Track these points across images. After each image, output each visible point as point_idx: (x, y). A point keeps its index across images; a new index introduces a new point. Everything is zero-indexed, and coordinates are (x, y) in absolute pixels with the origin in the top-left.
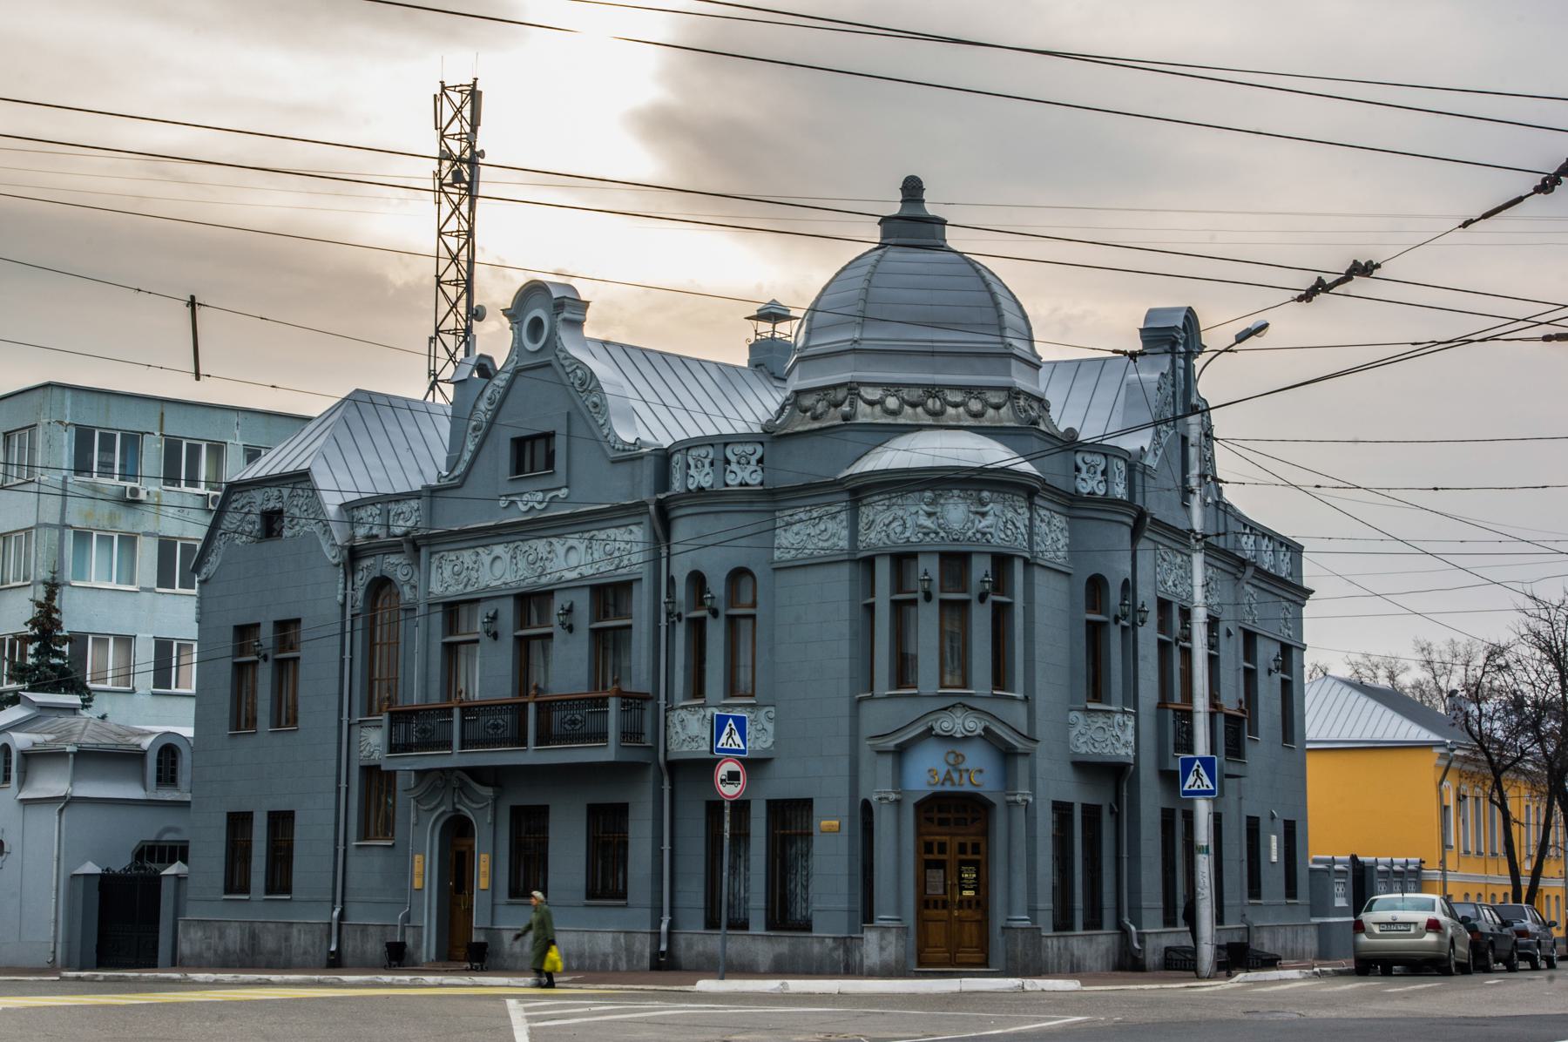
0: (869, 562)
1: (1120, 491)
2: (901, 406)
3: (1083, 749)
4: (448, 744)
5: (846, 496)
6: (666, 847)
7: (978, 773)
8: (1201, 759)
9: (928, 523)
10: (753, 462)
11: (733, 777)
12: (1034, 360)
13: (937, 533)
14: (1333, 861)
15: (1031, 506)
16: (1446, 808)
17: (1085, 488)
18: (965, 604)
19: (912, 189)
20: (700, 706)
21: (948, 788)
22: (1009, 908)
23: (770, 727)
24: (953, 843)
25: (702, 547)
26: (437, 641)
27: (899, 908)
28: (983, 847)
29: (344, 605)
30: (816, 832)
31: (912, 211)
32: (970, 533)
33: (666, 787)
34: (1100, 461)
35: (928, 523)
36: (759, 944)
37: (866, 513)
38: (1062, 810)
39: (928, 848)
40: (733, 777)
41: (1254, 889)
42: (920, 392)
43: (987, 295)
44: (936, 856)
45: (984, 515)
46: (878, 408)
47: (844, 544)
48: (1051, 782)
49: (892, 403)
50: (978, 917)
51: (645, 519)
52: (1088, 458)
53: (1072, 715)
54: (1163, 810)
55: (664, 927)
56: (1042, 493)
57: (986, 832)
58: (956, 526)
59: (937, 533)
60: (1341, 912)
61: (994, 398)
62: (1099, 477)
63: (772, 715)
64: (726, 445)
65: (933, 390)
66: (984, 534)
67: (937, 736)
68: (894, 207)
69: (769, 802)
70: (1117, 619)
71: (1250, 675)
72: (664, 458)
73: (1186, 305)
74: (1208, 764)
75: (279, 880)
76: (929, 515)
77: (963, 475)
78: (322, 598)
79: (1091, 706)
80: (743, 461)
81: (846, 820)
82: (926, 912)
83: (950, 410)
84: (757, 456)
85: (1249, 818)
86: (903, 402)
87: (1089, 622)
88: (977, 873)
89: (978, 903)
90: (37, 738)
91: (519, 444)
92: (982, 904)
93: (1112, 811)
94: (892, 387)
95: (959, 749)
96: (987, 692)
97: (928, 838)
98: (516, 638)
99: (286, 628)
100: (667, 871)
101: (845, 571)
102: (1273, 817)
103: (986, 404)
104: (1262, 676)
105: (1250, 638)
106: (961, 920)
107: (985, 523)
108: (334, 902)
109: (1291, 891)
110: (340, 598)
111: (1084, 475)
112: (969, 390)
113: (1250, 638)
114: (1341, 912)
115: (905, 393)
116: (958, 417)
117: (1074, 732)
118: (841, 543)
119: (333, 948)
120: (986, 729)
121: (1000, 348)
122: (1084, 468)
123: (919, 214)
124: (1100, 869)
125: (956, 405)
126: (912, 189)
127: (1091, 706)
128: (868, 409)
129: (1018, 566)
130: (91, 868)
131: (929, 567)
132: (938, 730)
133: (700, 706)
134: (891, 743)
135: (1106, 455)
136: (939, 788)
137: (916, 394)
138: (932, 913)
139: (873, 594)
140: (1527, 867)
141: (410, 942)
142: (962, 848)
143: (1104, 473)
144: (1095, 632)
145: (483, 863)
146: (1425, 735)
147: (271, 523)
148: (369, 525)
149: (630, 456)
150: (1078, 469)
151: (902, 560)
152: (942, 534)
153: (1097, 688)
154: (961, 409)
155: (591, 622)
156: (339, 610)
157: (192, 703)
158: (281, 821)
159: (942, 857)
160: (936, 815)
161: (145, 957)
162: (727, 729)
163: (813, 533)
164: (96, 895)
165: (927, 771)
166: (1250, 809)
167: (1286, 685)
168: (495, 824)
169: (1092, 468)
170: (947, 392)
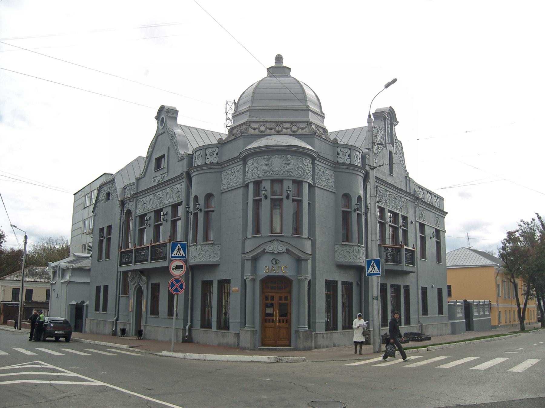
0: (247, 185)
1: (358, 162)
2: (266, 130)
3: (341, 260)
4: (131, 263)
6: (190, 298)
7: (285, 268)
8: (374, 260)
9: (266, 168)
10: (347, 156)
11: (179, 267)
12: (322, 115)
13: (270, 172)
14: (457, 302)
15: (313, 163)
16: (498, 285)
17: (341, 161)
19: (279, 59)
20: (195, 245)
22: (298, 322)
23: (219, 252)
24: (277, 296)
27: (253, 322)
28: (289, 298)
30: (231, 292)
31: (279, 65)
32: (282, 172)
33: (190, 276)
34: (347, 150)
35: (266, 168)
39: (267, 298)
40: (179, 267)
41: (425, 311)
42: (274, 124)
43: (301, 90)
44: (269, 301)
45: (288, 164)
46: (257, 131)
47: (241, 180)
48: (324, 271)
49: (262, 128)
50: (287, 326)
51: (184, 180)
52: (343, 150)
53: (336, 247)
54: (382, 285)
55: (187, 327)
56: (318, 159)
57: (290, 292)
58: (277, 169)
59: (270, 172)
60: (460, 318)
61: (302, 125)
62: (347, 157)
64: (206, 149)
65: (278, 123)
66: (289, 172)
68: (273, 63)
69: (218, 280)
70: (355, 211)
71: (423, 239)
72: (191, 158)
73: (389, 106)
74: (377, 262)
75: (105, 309)
76: (267, 165)
78: (115, 217)
79: (344, 243)
80: (212, 154)
82: (266, 324)
84: (216, 152)
85: (327, 282)
86: (267, 128)
87: (343, 211)
93: (357, 284)
94: (263, 123)
96: (290, 235)
97: (267, 294)
98: (155, 225)
99: (109, 228)
100: (189, 306)
102: (432, 287)
103: (299, 128)
104: (428, 241)
105: (422, 226)
106: (279, 327)
107: (288, 167)
108: (115, 314)
109: (441, 311)
111: (341, 156)
112: (292, 123)
113: (422, 226)
114: (460, 318)
115: (268, 125)
116: (287, 132)
117: (337, 253)
118: (240, 180)
120: (287, 250)
121: (305, 108)
122: (341, 153)
123: (281, 66)
124: (352, 306)
125: (287, 129)
126: (279, 59)
127: (344, 243)
128: (253, 131)
129: (305, 187)
130: (74, 302)
131: (266, 185)
132: (267, 250)
133: (195, 245)
134: (250, 256)
135: (350, 149)
136: (269, 274)
137: (272, 125)
138: (267, 324)
139: (248, 200)
140: (522, 306)
142: (280, 298)
143: (349, 155)
144: (346, 216)
145: (144, 301)
146: (491, 263)
147: (108, 194)
150: (338, 154)
151: (257, 184)
153: (347, 238)
154: (289, 130)
157: (22, 247)
158: (106, 288)
159: (272, 302)
162: (177, 248)
164: (75, 310)
165: (265, 268)
166: (422, 284)
167: (438, 244)
169: (344, 154)
170: (284, 124)
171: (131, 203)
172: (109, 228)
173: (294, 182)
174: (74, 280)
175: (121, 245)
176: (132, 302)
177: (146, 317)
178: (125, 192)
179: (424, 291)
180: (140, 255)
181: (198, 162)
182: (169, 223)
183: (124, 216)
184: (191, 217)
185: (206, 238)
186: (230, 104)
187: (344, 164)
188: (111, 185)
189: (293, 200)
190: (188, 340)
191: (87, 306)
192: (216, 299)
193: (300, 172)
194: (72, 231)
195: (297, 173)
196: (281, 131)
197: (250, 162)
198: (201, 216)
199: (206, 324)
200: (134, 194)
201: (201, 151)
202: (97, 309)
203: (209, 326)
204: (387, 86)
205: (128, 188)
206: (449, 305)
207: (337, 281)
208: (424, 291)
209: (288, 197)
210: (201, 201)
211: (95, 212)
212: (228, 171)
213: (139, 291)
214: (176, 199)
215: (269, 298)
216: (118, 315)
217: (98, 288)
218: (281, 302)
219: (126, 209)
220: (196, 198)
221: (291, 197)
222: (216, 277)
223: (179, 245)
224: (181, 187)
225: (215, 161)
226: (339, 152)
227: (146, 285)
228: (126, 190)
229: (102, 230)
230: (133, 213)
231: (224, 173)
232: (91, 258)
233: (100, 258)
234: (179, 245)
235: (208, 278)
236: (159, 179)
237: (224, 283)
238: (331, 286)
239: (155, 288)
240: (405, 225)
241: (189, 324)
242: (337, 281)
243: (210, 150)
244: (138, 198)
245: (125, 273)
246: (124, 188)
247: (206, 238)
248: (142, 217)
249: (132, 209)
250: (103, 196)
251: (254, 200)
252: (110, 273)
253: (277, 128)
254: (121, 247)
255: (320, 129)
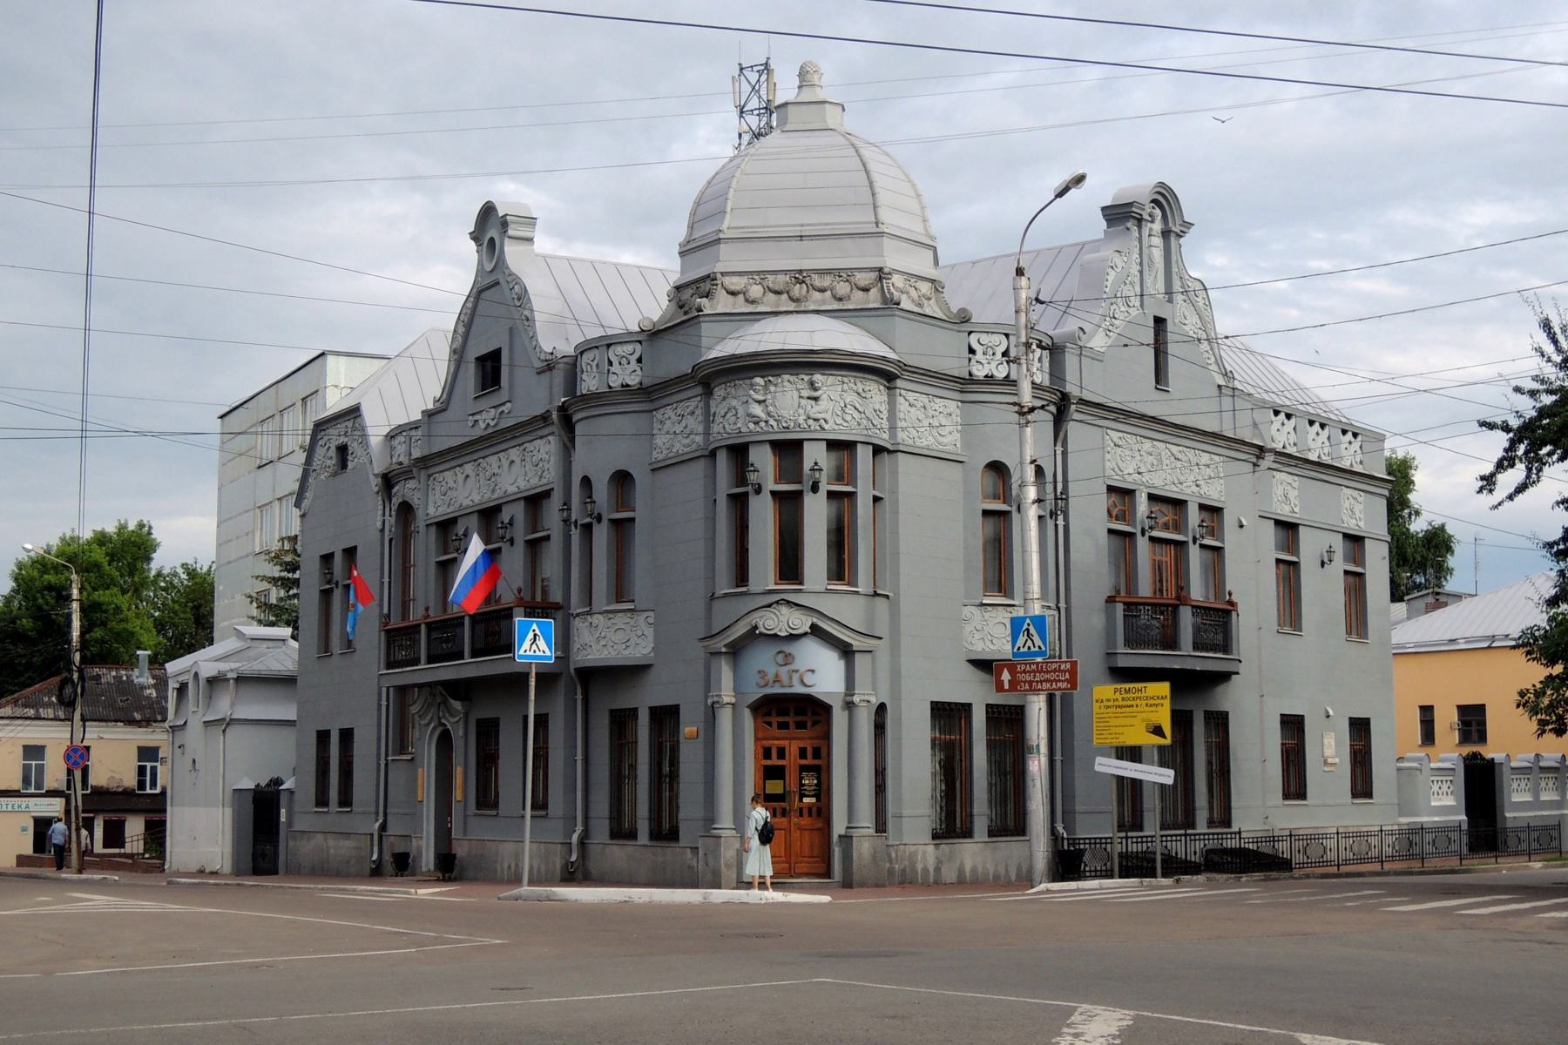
0: (713, 454)
4: (416, 661)
5: (699, 390)
6: (579, 757)
10: (999, 355)
17: (980, 373)
18: (800, 494)
21: (778, 690)
23: (649, 632)
24: (793, 748)
25: (603, 447)
26: (435, 558)
28: (824, 752)
29: (382, 531)
33: (579, 697)
36: (640, 850)
37: (718, 407)
38: (948, 715)
39: (767, 753)
44: (774, 761)
50: (820, 825)
52: (985, 338)
53: (967, 611)
55: (575, 837)
57: (827, 736)
63: (651, 620)
64: (609, 346)
65: (800, 277)
66: (816, 420)
67: (761, 634)
69: (651, 708)
72: (572, 368)
75: (346, 800)
77: (461, 330)
78: (368, 523)
81: (702, 726)
83: (817, 295)
84: (637, 355)
88: (819, 779)
89: (819, 811)
90: (237, 665)
91: (481, 360)
92: (823, 812)
95: (788, 648)
97: (767, 743)
99: (350, 553)
101: (702, 462)
104: (1310, 578)
107: (816, 408)
108: (377, 813)
110: (379, 525)
111: (979, 356)
116: (824, 302)
117: (968, 628)
119: (375, 857)
125: (822, 290)
130: (249, 784)
135: (1007, 335)
141: (1296, 873)
142: (803, 753)
145: (458, 772)
147: (343, 450)
148: (401, 454)
149: (549, 366)
150: (972, 351)
152: (772, 422)
155: (526, 534)
156: (378, 535)
158: (347, 736)
159: (781, 762)
160: (775, 720)
161: (272, 871)
163: (677, 430)
168: (466, 734)
171: (411, 484)
172: (350, 553)
173: (833, 445)
174: (242, 712)
175: (386, 611)
176: (427, 775)
177: (466, 817)
178: (392, 448)
179: (1293, 726)
180: (444, 636)
181: (590, 383)
182: (520, 547)
183: (391, 520)
184: (576, 534)
185: (620, 591)
186: (753, 77)
187: (989, 379)
188: (349, 424)
189: (832, 495)
190: (575, 874)
191: (291, 792)
192: (647, 760)
193: (848, 418)
194: (219, 545)
195: (839, 421)
196: (806, 299)
197: (719, 392)
198: (601, 534)
199: (622, 832)
200: (418, 460)
201: (596, 351)
202: (322, 800)
203: (632, 835)
204: (1060, 194)
205: (401, 439)
206: (1399, 769)
207: (970, 705)
208: (1293, 726)
209: (815, 488)
210: (601, 492)
211: (305, 504)
212: (669, 412)
213: (445, 740)
214: (534, 481)
215: (774, 753)
216: (385, 815)
217: (323, 737)
218: (768, 762)
219: (396, 501)
220: (586, 482)
221: (824, 487)
222: (646, 697)
223: (535, 626)
224: (547, 448)
225: (633, 381)
226: (975, 346)
227: (461, 724)
228: (395, 443)
229: (327, 559)
230: (420, 514)
231: (658, 415)
232: (295, 644)
233: (326, 648)
234: (535, 626)
235: (623, 701)
236: (488, 419)
237: (666, 717)
238: (948, 715)
239: (488, 733)
240: (1215, 529)
241: (579, 829)
242: (970, 705)
243: (620, 350)
244: (431, 471)
245: (402, 690)
246: (391, 436)
247: (620, 591)
248: (445, 527)
249: (415, 500)
250: (326, 457)
251: (730, 496)
252: (360, 692)
253: (795, 291)
254: (389, 616)
255: (920, 284)
